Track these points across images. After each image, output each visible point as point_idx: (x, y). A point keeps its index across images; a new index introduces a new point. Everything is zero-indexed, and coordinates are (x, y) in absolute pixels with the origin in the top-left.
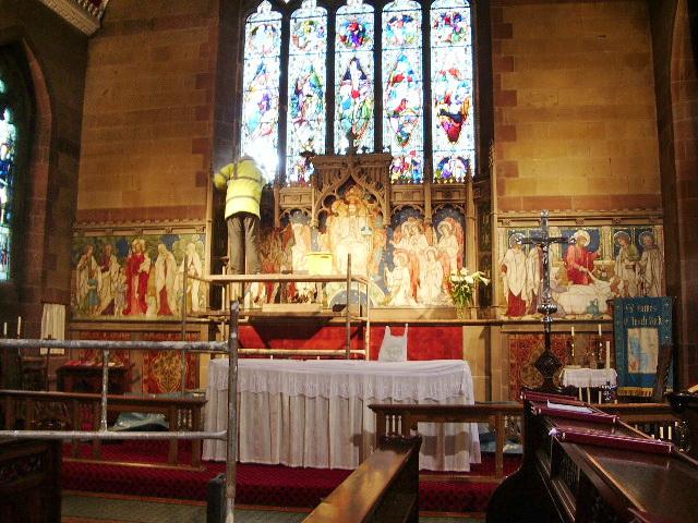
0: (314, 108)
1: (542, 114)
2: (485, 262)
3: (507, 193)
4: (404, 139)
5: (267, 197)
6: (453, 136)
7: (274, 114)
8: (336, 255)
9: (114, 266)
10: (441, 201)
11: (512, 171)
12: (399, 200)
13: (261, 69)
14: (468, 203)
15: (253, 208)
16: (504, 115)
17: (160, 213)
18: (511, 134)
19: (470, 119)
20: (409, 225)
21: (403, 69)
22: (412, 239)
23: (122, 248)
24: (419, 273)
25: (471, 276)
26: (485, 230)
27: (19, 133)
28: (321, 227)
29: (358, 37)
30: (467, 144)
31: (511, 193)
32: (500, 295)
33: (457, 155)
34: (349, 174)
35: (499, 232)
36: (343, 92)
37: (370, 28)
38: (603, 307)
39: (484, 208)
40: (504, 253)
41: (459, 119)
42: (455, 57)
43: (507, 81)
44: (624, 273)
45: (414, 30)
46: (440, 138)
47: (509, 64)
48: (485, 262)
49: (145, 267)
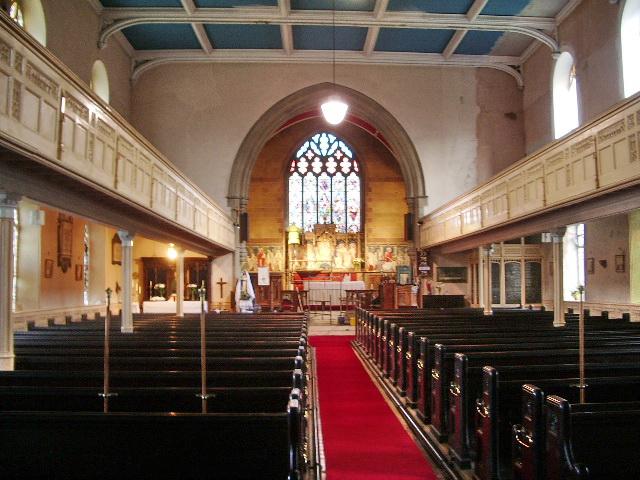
0: (312, 207)
1: (379, 215)
2: (363, 256)
3: (368, 237)
4: (339, 219)
5: (301, 236)
6: (353, 219)
7: (300, 210)
8: (319, 256)
9: (253, 255)
10: (351, 238)
11: (370, 231)
12: (338, 238)
13: (295, 195)
14: (359, 239)
15: (298, 241)
16: (369, 215)
17: (267, 241)
18: (370, 220)
19: (359, 214)
20: (341, 245)
21: (338, 198)
22: (342, 249)
23: (256, 251)
24: (345, 258)
25: (359, 260)
26: (363, 247)
27: (489, 317)
28: (316, 245)
29: (325, 187)
30: (357, 221)
31: (371, 237)
32: (367, 265)
33: (355, 225)
34: (325, 230)
35: (367, 248)
36: (321, 204)
37: (329, 184)
38: (394, 268)
39: (363, 240)
40: (368, 254)
41: (355, 214)
42: (355, 194)
43: (369, 205)
44: (400, 259)
45: (342, 185)
46: (349, 219)
47: (370, 200)
48: (363, 256)
49: (264, 256)
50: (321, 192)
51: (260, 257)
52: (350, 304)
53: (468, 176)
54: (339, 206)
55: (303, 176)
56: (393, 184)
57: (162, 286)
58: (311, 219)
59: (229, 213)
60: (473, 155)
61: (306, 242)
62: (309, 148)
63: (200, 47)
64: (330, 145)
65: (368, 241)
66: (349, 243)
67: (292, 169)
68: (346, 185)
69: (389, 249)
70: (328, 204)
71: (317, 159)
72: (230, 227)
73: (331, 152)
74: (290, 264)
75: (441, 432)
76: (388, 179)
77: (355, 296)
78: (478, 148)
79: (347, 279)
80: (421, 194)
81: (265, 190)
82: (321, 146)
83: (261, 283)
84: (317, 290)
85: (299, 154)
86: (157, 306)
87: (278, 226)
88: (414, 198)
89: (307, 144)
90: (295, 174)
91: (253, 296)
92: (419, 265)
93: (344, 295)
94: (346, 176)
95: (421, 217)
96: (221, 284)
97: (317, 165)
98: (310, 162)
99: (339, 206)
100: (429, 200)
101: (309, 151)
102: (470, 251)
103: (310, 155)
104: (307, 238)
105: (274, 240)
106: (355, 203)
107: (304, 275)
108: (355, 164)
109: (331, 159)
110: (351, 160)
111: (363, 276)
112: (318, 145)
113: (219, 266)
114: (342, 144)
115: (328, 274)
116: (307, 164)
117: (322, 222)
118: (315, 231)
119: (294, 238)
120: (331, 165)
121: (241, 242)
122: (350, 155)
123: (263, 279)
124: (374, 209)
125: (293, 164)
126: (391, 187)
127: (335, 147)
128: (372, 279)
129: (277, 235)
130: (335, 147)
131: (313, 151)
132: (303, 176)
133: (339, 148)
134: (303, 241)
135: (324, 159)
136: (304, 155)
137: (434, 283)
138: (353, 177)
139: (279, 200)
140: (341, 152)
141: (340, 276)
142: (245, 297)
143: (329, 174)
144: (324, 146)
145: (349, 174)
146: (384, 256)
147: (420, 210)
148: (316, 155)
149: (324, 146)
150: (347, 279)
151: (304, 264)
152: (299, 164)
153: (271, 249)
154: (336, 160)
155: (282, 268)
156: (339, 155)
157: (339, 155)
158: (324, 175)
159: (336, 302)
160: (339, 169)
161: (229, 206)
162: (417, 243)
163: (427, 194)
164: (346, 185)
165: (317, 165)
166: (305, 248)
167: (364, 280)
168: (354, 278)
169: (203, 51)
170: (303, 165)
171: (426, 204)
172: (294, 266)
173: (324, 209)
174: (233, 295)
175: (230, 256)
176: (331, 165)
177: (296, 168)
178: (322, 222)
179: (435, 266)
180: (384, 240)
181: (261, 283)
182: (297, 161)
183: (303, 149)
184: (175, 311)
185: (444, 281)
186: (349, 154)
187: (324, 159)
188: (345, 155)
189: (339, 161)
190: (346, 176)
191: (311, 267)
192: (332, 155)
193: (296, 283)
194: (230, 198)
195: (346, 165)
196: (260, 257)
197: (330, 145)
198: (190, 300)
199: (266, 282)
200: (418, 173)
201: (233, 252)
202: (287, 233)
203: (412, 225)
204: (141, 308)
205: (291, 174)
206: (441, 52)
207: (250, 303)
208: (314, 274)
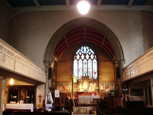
0: (81, 70)
1: (104, 73)
2: (98, 87)
3: (100, 80)
5: (77, 80)
8: (83, 87)
9: (61, 87)
10: (94, 81)
11: (101, 78)
12: (90, 81)
14: (97, 81)
15: (76, 81)
16: (100, 73)
17: (66, 82)
18: (101, 75)
20: (91, 83)
21: (90, 67)
22: (91, 84)
23: (62, 85)
24: (92, 88)
25: (97, 88)
26: (98, 84)
28: (83, 83)
29: (86, 64)
30: (96, 75)
31: (101, 80)
32: (100, 90)
33: (95, 76)
34: (85, 78)
35: (100, 84)
36: (84, 69)
39: (98, 82)
40: (100, 86)
41: (96, 73)
43: (100, 69)
44: (111, 87)
49: (65, 87)
50: (84, 65)
51: (63, 87)
52: (94, 104)
53: (141, 51)
54: (90, 70)
55: (78, 60)
56: (108, 62)
57: (15, 97)
58: (81, 75)
59: (44, 68)
60: (142, 43)
61: (79, 82)
62: (80, 51)
63: (35, 5)
64: (87, 50)
65: (100, 82)
66: (94, 82)
67: (75, 58)
68: (92, 63)
69: (107, 84)
70: (87, 70)
71: (83, 55)
72: (44, 74)
73: (87, 52)
74: (74, 90)
75: (104, 99)
76: (106, 61)
77: (96, 101)
78: (144, 40)
79: (93, 94)
80: (122, 59)
81: (66, 65)
82: (84, 51)
83: (56, 96)
84: (82, 99)
85: (77, 53)
86: (13, 105)
87: (70, 77)
88: (119, 61)
89: (79, 50)
90: (76, 60)
91: (52, 101)
92: (123, 88)
93: (92, 100)
94: (92, 60)
95: (123, 68)
96: (40, 97)
97: (83, 57)
98: (80, 56)
99: (90, 70)
100: (126, 61)
101: (80, 52)
102: (145, 82)
103: (80, 53)
104: (79, 81)
105: (68, 82)
106: (95, 69)
107: (78, 93)
108: (95, 56)
109: (87, 55)
110: (94, 55)
111: (99, 94)
112: (83, 50)
113: (39, 89)
114: (91, 50)
115: (87, 93)
116: (79, 56)
118: (82, 78)
119: (75, 81)
120: (87, 57)
121: (49, 79)
122: (94, 53)
124: (102, 71)
125: (75, 57)
126: (109, 64)
127: (88, 51)
128: (102, 95)
129: (69, 80)
130: (88, 51)
131: (81, 52)
132: (78, 60)
133: (90, 51)
134: (78, 82)
135: (85, 55)
136: (78, 53)
137: (130, 96)
138: (95, 61)
139: (70, 68)
140: (91, 52)
141: (91, 94)
142: (49, 102)
143: (86, 59)
144: (85, 50)
145: (93, 59)
146: (106, 87)
147: (122, 65)
148: (82, 53)
149: (85, 50)
150: (93, 94)
151: (78, 89)
152: (77, 57)
153: (67, 84)
154: (89, 55)
155: (71, 91)
156: (90, 53)
157: (90, 53)
158: (85, 60)
159: (89, 103)
160: (90, 58)
161: (44, 64)
162: (122, 79)
163: (125, 59)
164: (92, 63)
165: (83, 57)
166: (79, 84)
167: (99, 95)
168: (95, 94)
169: (37, 7)
170: (78, 57)
171: (125, 63)
172: (75, 90)
173: (85, 71)
174: (44, 101)
175: (44, 85)
176: (87, 57)
177: (76, 58)
179: (129, 89)
180: (105, 81)
181: (56, 96)
182: (76, 55)
183: (78, 51)
185: (134, 95)
186: (93, 53)
187: (85, 55)
188: (92, 53)
189: (90, 55)
190: (92, 60)
191: (81, 91)
192: (88, 53)
193: (76, 96)
194: (44, 61)
195: (92, 57)
196: (63, 87)
197: (87, 50)
198: (27, 103)
199: (58, 96)
200: (121, 50)
201: (45, 84)
202: (73, 79)
203: (119, 72)
205: (74, 60)
206: (127, 5)
207: (51, 105)
208: (82, 93)
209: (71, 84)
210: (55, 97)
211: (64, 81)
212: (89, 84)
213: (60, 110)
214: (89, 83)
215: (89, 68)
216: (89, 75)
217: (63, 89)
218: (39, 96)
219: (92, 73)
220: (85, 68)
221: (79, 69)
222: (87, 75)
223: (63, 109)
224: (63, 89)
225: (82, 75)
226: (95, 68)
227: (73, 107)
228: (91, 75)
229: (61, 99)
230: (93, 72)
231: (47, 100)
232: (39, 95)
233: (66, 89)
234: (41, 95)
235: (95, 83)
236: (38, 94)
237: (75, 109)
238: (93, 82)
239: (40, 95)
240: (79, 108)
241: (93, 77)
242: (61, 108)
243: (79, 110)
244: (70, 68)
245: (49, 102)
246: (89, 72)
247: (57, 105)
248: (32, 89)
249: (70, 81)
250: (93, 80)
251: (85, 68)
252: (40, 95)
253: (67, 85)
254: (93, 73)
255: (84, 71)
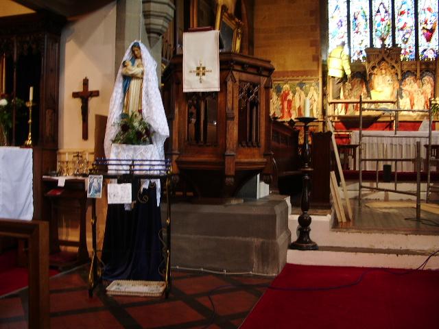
0: (363, 23)
6: (429, 39)
7: (345, 28)
20: (409, 80)
21: (404, 8)
22: (410, 86)
34: (385, 56)
36: (377, 19)
46: (422, 40)
49: (290, 97)
51: (284, 97)
58: (361, 41)
83: (191, 83)
87: (311, 52)
96: (85, 96)
105: (305, 73)
113: (81, 43)
117: (378, 44)
118: (368, 59)
123: (201, 71)
139: (312, 13)
142: (135, 133)
153: (301, 85)
155: (317, 114)
159: (407, 168)
173: (381, 26)
178: (378, 44)
181: (191, 83)
184: (398, 185)
199: (211, 82)
204: (396, 186)
207: (151, 156)
209: (318, 84)
210: (185, 90)
211: (287, 72)
212: (401, 81)
213: (234, 192)
214: (400, 77)
215: (402, 13)
216: (399, 41)
217: (282, 104)
218: (75, 95)
219: (414, 32)
220: (382, 11)
221: (352, 19)
222: (388, 42)
223: (263, 190)
224: (282, 104)
225: (367, 43)
226: (429, 10)
227: (333, 174)
228: (412, 41)
229: (233, 103)
230: (420, 28)
231: (124, 116)
232: (79, 89)
233: (297, 107)
234: (91, 88)
235: (428, 79)
236: (70, 83)
237: (425, 48)
238: (418, 75)
239: (86, 82)
240: (361, 187)
241: (421, 50)
242: (230, 180)
243: (358, 200)
244: (312, 13)
245: (135, 133)
246: (402, 29)
247: (203, 158)
248: (26, 46)
249: (316, 68)
250: (421, 64)
251: (382, 11)
252: (86, 82)
253: (298, 88)
254: (420, 33)
255: (375, 27)
